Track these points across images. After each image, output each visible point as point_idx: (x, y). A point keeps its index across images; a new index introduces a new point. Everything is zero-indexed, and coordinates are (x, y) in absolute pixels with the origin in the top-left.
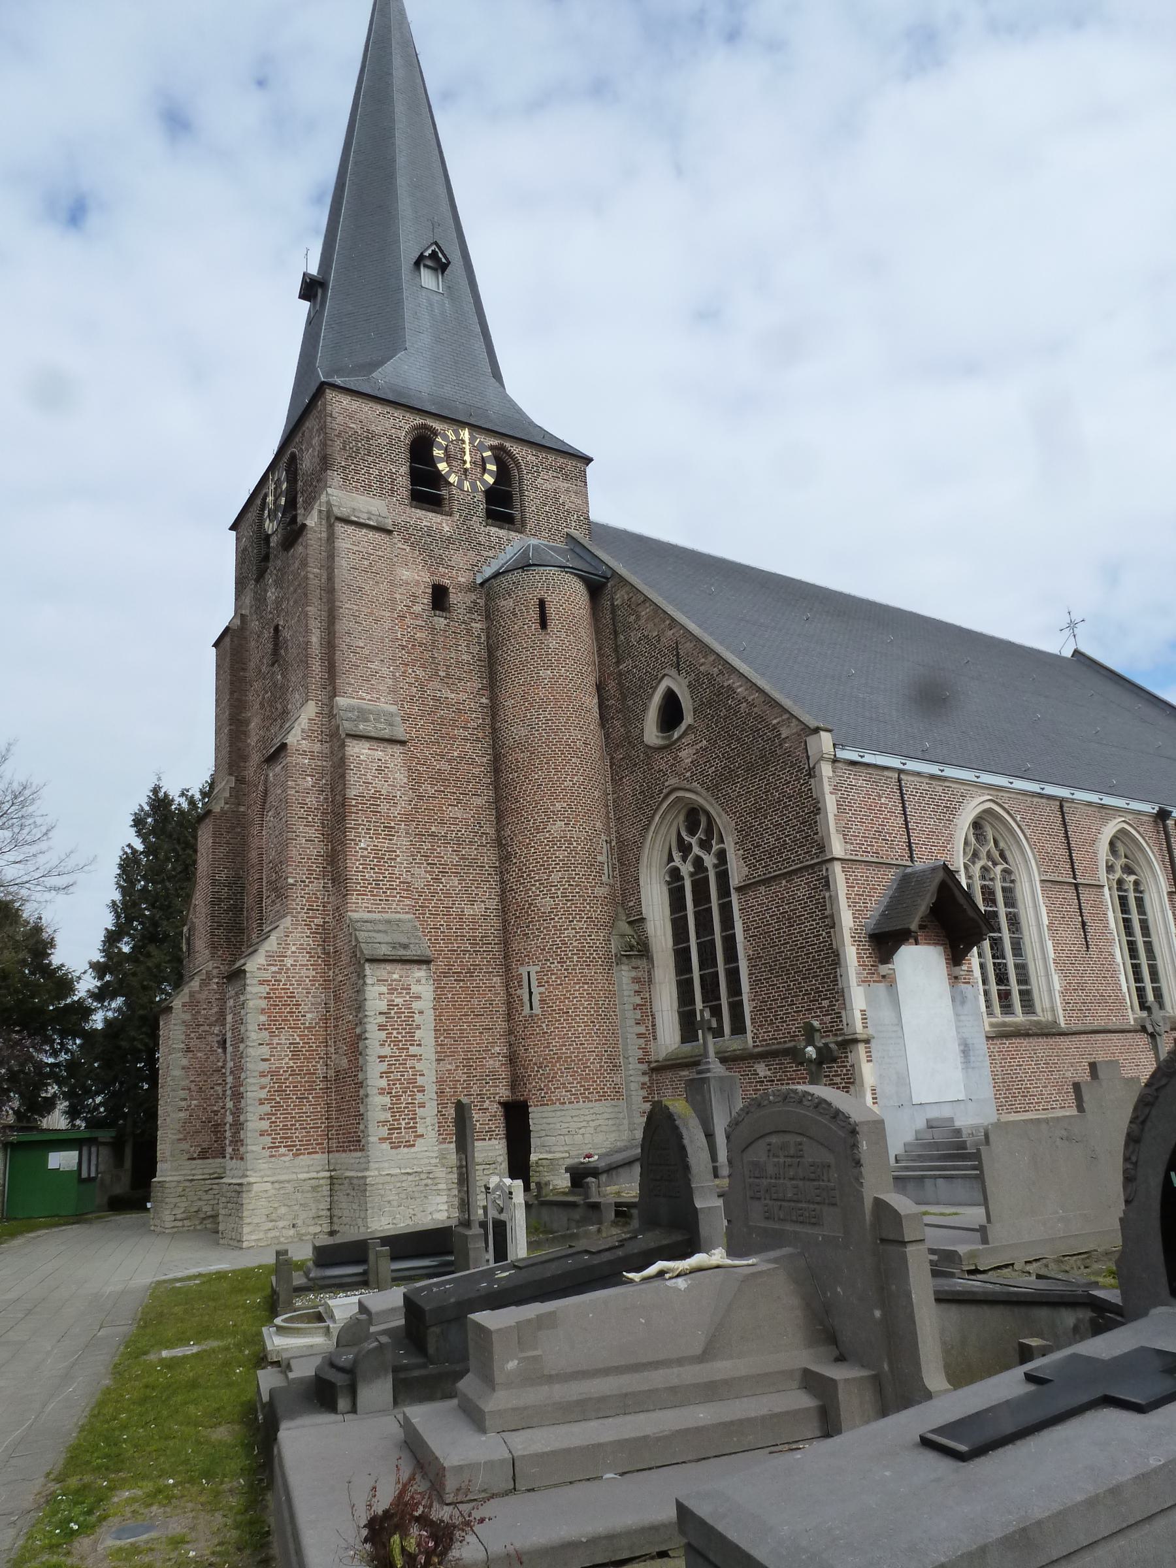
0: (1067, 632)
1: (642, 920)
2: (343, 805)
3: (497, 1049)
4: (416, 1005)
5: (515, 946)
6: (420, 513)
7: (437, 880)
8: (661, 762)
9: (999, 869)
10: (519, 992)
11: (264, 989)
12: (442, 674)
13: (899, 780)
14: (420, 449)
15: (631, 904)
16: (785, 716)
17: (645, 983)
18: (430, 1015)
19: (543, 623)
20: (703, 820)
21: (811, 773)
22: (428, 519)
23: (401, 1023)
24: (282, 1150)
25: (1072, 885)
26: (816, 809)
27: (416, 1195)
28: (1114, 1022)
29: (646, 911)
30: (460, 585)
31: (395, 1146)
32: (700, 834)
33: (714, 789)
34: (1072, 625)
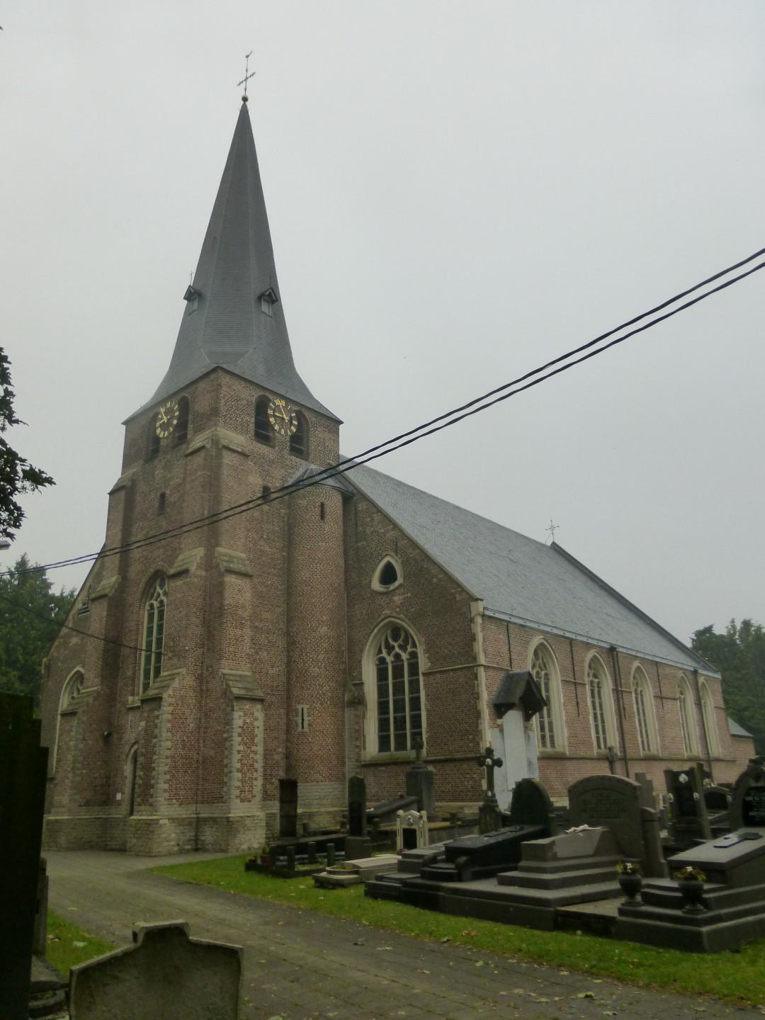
0: (549, 531)
1: (362, 684)
2: (220, 608)
3: (280, 750)
4: (256, 724)
6: (259, 445)
7: (257, 653)
9: (543, 673)
10: (295, 719)
11: (171, 709)
13: (508, 626)
14: (261, 407)
15: (355, 674)
16: (459, 589)
18: (262, 728)
19: (322, 516)
21: (472, 620)
22: (263, 449)
23: (248, 733)
24: (174, 801)
25: (573, 683)
28: (589, 754)
29: (365, 678)
32: (400, 641)
34: (552, 528)
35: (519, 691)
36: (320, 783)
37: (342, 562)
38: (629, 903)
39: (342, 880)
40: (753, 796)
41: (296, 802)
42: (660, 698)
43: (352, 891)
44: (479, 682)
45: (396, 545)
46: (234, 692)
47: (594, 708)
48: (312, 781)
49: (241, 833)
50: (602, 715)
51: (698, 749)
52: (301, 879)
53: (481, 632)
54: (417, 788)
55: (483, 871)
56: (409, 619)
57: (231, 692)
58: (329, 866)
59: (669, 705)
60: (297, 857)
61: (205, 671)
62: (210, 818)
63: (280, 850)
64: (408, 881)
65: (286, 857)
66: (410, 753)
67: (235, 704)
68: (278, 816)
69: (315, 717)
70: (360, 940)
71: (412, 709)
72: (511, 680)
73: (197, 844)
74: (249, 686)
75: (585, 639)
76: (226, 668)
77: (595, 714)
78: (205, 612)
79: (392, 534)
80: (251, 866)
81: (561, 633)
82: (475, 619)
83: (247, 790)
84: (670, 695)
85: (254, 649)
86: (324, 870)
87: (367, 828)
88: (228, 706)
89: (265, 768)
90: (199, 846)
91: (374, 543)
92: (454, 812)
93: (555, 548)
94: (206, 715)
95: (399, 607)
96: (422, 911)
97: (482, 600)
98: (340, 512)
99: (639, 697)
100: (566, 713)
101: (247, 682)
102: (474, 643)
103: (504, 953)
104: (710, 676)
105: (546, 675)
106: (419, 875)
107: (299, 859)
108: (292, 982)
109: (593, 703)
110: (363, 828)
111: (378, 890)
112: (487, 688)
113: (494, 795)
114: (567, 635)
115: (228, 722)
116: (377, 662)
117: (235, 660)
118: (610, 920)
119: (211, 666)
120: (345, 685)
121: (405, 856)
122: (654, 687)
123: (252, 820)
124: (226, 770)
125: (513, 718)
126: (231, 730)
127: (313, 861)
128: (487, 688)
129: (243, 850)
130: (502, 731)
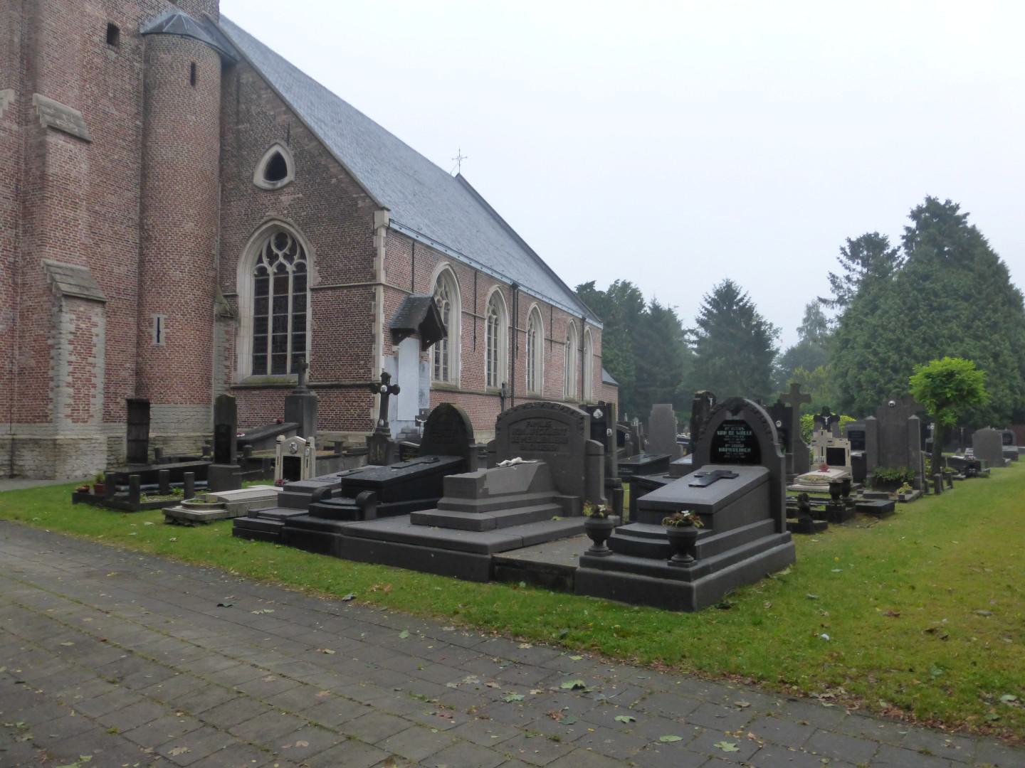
1: (235, 296)
3: (128, 365)
4: (94, 330)
5: (149, 299)
8: (266, 199)
9: (444, 302)
10: (149, 330)
12: (111, 95)
13: (413, 245)
15: (227, 284)
16: (363, 195)
17: (233, 336)
18: (102, 336)
19: (193, 80)
20: (290, 242)
21: (374, 232)
23: (83, 342)
25: (473, 317)
26: (374, 253)
27: (88, 453)
28: (479, 390)
29: (239, 290)
30: (128, 30)
31: (75, 421)
32: (286, 250)
33: (305, 225)
34: (460, 158)
35: (420, 317)
36: (179, 405)
37: (217, 146)
38: (594, 551)
39: (204, 516)
40: (727, 431)
41: (147, 424)
42: (550, 341)
43: (216, 530)
44: (377, 303)
45: (289, 132)
46: (63, 289)
47: (489, 345)
48: (169, 403)
49: (74, 457)
50: (495, 351)
51: (575, 392)
52: (146, 513)
53: (384, 247)
54: (297, 412)
55: (399, 508)
56: (299, 225)
57: (58, 289)
58: (186, 497)
59: (557, 347)
60: (142, 487)
61: (19, 259)
62: (30, 439)
63: (123, 479)
64: (294, 518)
65: (128, 487)
66: (290, 377)
67: (64, 303)
68: (125, 441)
69: (175, 325)
70: (226, 600)
71: (295, 328)
72: (411, 304)
73: (12, 469)
74: (83, 283)
75: (489, 272)
76: (50, 258)
77: (489, 350)
78: (19, 181)
79: (283, 118)
80: (81, 497)
81: (467, 261)
82: (379, 230)
83: (81, 408)
84: (560, 340)
85: (93, 239)
86: (178, 503)
87: (236, 455)
88: (53, 305)
89: (107, 387)
90: (15, 472)
91: (260, 127)
92: (340, 440)
93: (460, 179)
94: (22, 316)
95: (287, 209)
96: (310, 555)
97: (388, 210)
98: (218, 81)
99: (531, 338)
100: (463, 346)
101: (82, 278)
102: (374, 259)
103: (434, 616)
104: (595, 326)
105: (447, 304)
106: (307, 511)
107: (143, 490)
108: (113, 682)
109: (489, 339)
110: (229, 454)
111: (250, 529)
112: (384, 312)
113: (386, 424)
114: (473, 265)
115: (54, 326)
116: (256, 273)
117: (64, 249)
118: (569, 571)
119: (29, 254)
120: (214, 296)
121: (287, 488)
122: (546, 330)
123: (90, 446)
124: (52, 384)
125: (409, 346)
126: (59, 336)
127: (165, 491)
128: (384, 312)
129: (76, 477)
130: (396, 359)
